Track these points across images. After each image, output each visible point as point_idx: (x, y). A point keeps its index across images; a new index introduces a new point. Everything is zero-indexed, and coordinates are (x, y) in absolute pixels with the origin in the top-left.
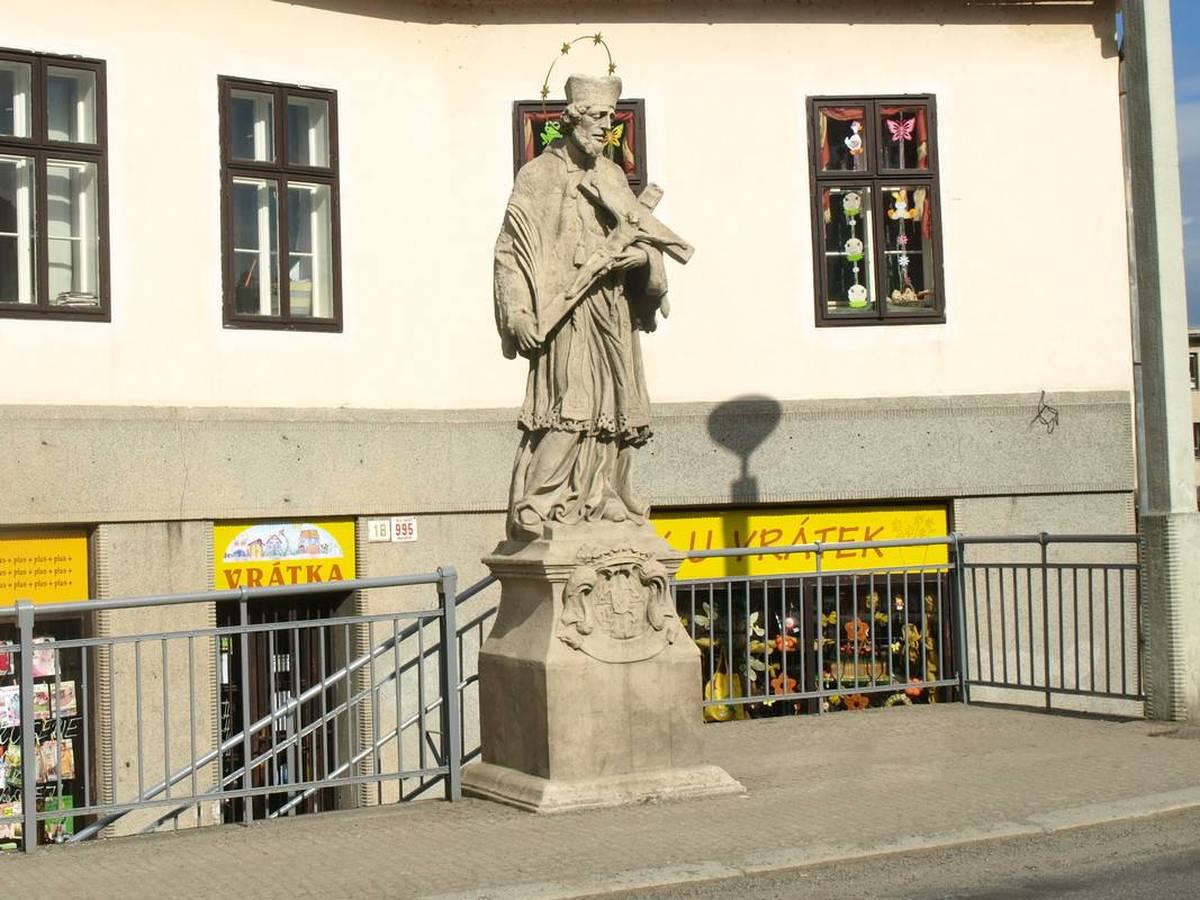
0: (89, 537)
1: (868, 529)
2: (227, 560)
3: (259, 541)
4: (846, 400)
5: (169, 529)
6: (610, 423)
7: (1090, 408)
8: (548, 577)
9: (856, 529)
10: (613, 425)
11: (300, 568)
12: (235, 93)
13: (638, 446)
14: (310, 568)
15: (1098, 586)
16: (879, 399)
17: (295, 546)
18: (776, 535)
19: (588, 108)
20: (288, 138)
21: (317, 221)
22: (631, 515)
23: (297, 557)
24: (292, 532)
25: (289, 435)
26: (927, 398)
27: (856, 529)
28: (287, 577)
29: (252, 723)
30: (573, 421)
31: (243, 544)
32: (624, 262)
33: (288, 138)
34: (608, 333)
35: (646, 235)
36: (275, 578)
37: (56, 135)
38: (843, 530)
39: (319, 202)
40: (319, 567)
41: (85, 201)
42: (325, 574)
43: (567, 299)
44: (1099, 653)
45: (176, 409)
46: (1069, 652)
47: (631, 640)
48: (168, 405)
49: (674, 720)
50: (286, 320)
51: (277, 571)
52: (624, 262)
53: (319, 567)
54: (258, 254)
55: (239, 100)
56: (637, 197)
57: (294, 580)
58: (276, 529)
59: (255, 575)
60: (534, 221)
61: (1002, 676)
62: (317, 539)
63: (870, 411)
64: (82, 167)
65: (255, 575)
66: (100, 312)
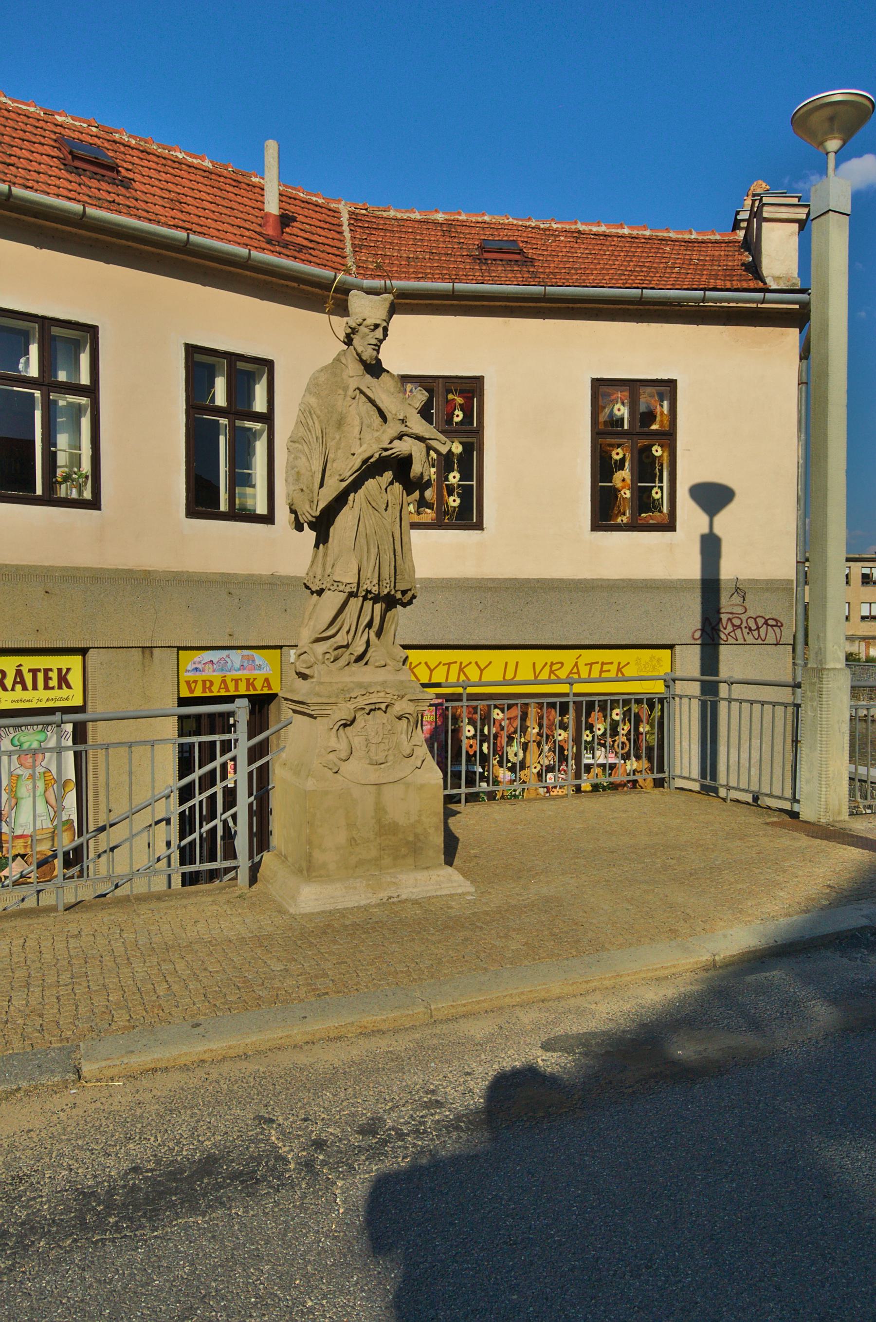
0: (84, 656)
1: (619, 663)
2: (189, 674)
3: (211, 661)
4: (608, 580)
5: (143, 653)
7: (767, 590)
9: (612, 663)
10: (376, 588)
11: (241, 679)
12: (198, 357)
13: (404, 605)
14: (248, 680)
15: (768, 718)
16: (630, 580)
17: (237, 665)
18: (559, 665)
19: (364, 320)
20: (240, 389)
21: (260, 447)
23: (240, 672)
24: (236, 657)
25: (232, 591)
26: (661, 580)
27: (612, 663)
28: (231, 686)
31: (199, 663)
32: (390, 452)
33: (240, 389)
35: (411, 431)
36: (223, 686)
37: (62, 376)
38: (603, 664)
39: (261, 435)
40: (255, 679)
41: (85, 423)
42: (258, 684)
43: (342, 481)
44: (766, 748)
45: (149, 572)
46: (745, 746)
47: (382, 766)
48: (144, 568)
49: (419, 830)
50: (241, 514)
51: (224, 681)
52: (390, 452)
53: (255, 679)
54: (250, 475)
55: (200, 363)
56: (250, 886)
57: (237, 689)
58: (225, 653)
59: (208, 684)
60: (318, 417)
62: (254, 661)
63: (623, 588)
64: (84, 401)
65: (208, 684)
66: (95, 504)
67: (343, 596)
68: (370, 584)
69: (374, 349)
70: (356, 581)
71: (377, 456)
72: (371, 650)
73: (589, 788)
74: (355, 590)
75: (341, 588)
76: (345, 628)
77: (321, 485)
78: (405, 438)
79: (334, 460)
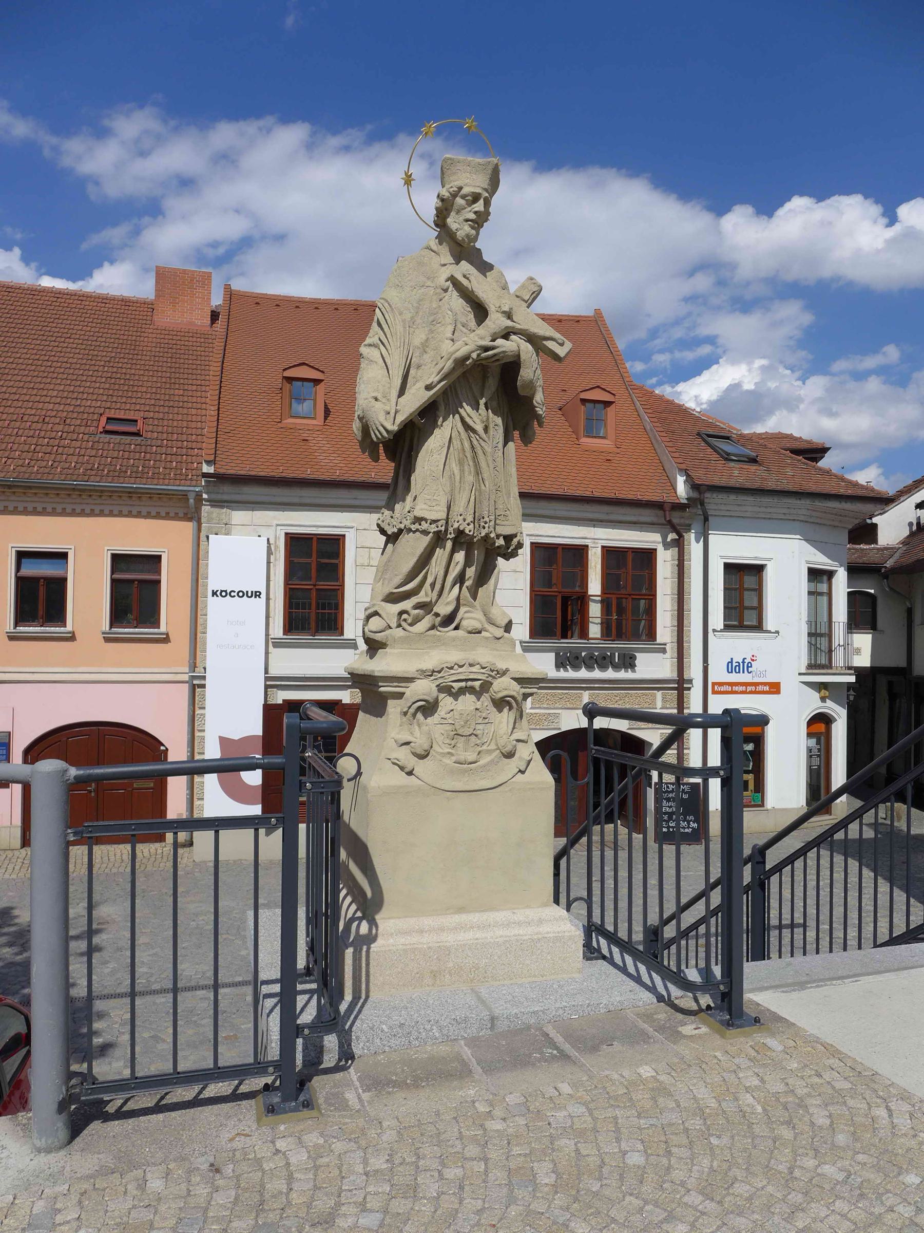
6: (468, 524)
8: (382, 689)
22: (487, 626)
29: (588, 783)
30: (426, 520)
34: (474, 431)
35: (518, 326)
56: (829, 449)
61: (912, 817)
67: (426, 540)
68: (462, 520)
69: (473, 228)
70: (444, 516)
71: (474, 355)
72: (462, 610)
73: (22, 509)
74: (443, 529)
75: (425, 526)
76: (430, 580)
77: (402, 392)
78: (513, 337)
79: (419, 367)
